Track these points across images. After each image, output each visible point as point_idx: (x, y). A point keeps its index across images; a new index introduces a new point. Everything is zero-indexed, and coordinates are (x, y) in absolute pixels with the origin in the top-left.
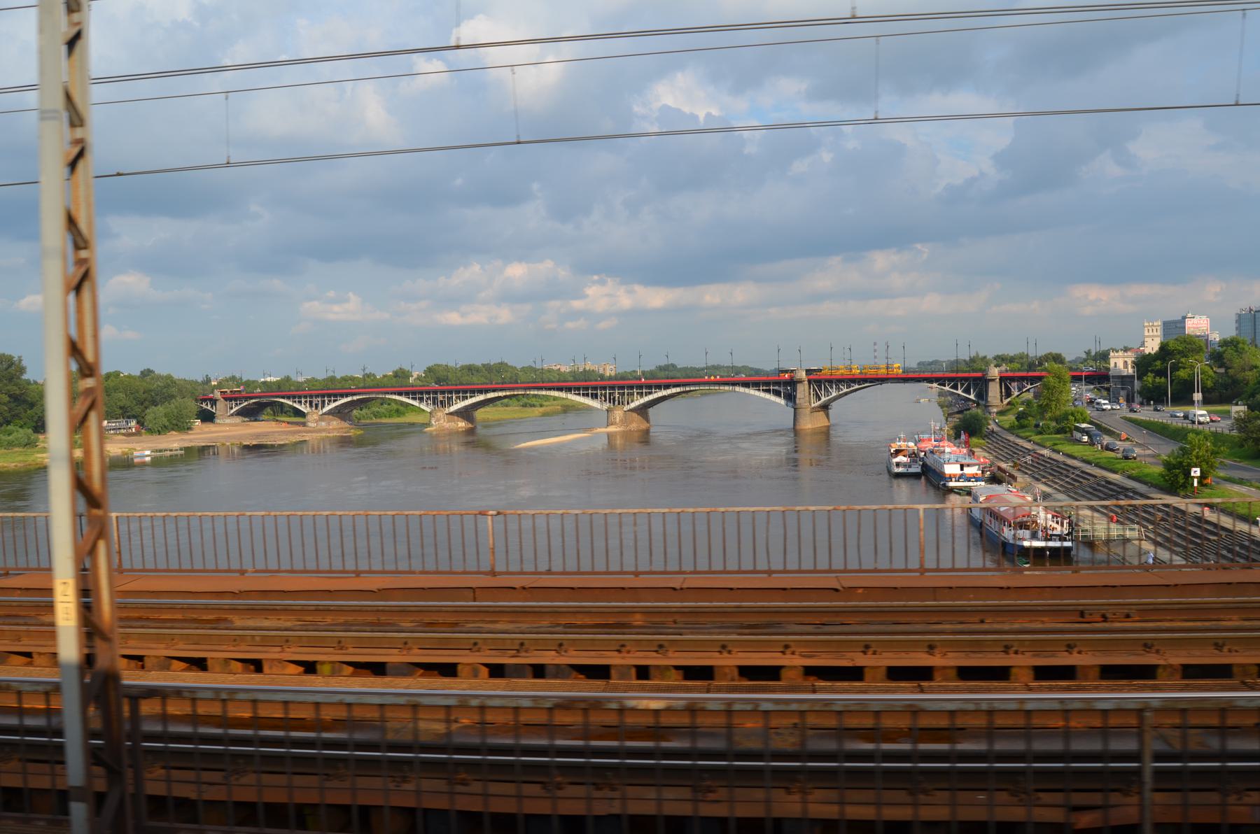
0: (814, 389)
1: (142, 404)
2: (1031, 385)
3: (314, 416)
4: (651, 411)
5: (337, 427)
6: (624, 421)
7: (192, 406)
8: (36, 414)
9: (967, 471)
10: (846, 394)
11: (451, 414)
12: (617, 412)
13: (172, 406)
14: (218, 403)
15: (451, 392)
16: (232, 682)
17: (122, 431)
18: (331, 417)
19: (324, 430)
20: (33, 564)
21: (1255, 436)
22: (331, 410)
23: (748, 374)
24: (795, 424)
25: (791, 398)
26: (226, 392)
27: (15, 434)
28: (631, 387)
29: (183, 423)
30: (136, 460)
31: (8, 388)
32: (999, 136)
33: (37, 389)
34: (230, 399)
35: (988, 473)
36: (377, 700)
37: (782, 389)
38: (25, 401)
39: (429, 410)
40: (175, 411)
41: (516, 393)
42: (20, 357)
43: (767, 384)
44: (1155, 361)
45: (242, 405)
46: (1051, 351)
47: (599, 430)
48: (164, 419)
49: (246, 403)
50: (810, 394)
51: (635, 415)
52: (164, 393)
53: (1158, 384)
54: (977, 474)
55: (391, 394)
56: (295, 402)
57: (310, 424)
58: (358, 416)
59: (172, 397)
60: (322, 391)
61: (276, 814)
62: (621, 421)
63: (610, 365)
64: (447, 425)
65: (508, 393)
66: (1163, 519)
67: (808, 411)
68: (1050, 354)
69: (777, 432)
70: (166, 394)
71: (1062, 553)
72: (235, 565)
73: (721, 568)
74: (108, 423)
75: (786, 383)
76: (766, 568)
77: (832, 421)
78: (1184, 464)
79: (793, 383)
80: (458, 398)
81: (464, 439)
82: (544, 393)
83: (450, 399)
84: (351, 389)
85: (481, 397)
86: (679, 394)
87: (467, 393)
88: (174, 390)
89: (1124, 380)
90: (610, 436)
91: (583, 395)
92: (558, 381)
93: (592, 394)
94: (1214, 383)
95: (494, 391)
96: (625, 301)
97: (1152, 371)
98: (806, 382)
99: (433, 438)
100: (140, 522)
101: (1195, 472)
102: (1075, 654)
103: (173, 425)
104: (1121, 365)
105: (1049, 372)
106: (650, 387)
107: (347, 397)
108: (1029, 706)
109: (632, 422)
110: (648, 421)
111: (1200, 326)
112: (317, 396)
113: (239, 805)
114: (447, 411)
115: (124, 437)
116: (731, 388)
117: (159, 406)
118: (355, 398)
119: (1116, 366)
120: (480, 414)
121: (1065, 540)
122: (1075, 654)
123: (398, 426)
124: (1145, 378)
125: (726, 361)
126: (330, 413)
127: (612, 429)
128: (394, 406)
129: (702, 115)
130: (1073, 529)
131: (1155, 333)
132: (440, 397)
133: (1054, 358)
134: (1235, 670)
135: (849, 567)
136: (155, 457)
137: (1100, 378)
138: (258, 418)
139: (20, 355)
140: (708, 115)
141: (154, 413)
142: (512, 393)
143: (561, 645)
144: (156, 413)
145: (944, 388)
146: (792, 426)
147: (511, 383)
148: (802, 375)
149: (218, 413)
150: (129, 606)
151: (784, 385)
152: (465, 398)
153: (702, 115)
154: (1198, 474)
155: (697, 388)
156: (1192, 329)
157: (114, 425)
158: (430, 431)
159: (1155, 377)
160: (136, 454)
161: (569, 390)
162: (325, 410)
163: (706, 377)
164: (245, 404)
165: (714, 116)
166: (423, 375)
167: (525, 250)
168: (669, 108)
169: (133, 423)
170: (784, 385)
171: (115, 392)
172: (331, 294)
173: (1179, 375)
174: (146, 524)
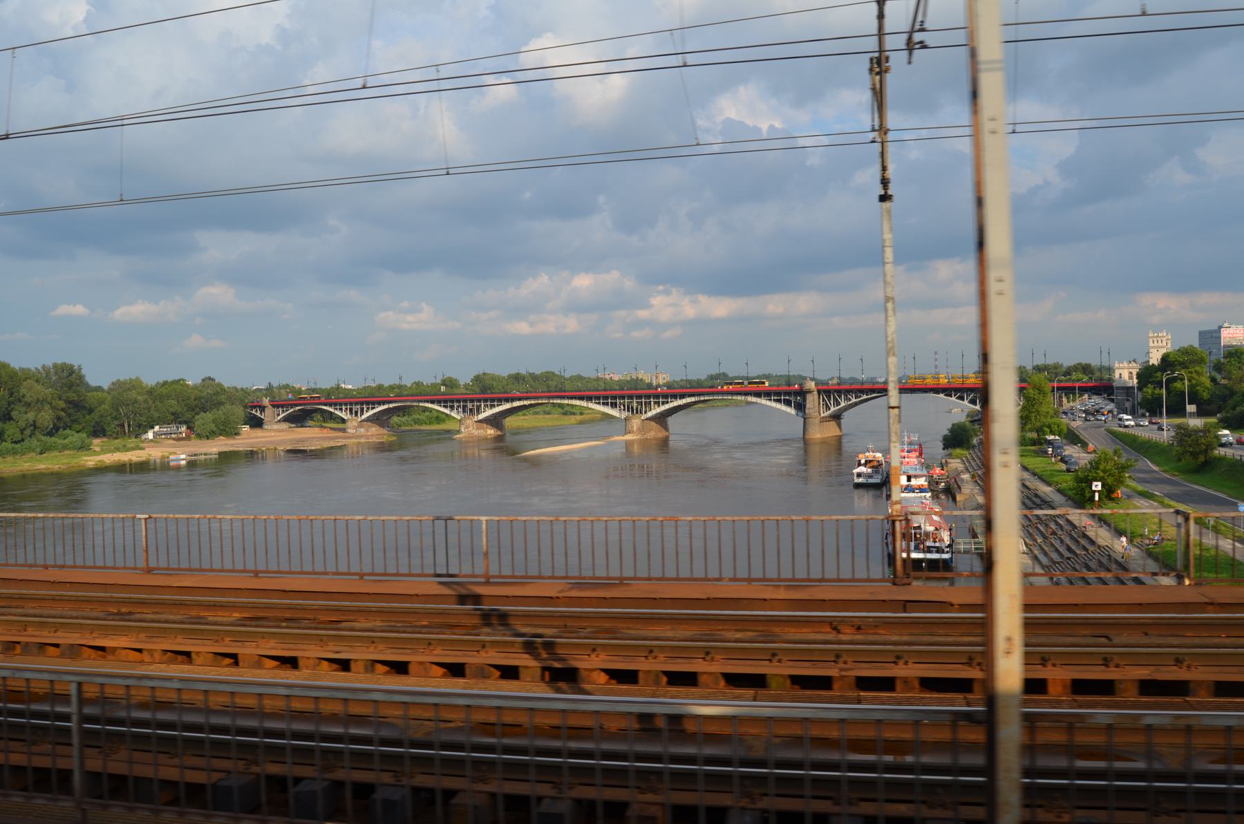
0: (824, 400)
1: (193, 410)
2: (867, 395)
3: (353, 422)
4: (670, 420)
5: (375, 434)
6: (642, 430)
8: (94, 419)
9: (914, 482)
10: (856, 404)
11: (480, 421)
13: (220, 413)
14: (266, 410)
15: (479, 401)
16: (188, 672)
17: (173, 436)
18: (369, 423)
19: (361, 436)
20: (79, 562)
21: (1191, 450)
22: (369, 417)
23: (521, 391)
24: (804, 434)
25: (800, 407)
27: (70, 437)
28: (648, 397)
29: (230, 428)
30: (172, 464)
31: (68, 394)
32: (1065, 146)
33: (97, 395)
34: (278, 407)
35: (943, 484)
36: (229, 688)
37: (792, 399)
38: (84, 408)
39: (459, 418)
40: (223, 417)
41: (540, 402)
42: (79, 366)
43: (778, 394)
44: (1156, 372)
45: (288, 412)
46: (1081, 361)
47: (616, 438)
48: (211, 424)
49: (292, 410)
50: (819, 404)
51: (653, 423)
52: (213, 400)
53: (1157, 396)
54: (922, 485)
55: (425, 402)
56: (337, 409)
57: (349, 430)
58: (399, 423)
59: (222, 404)
62: (639, 429)
63: (663, 374)
64: (476, 432)
65: (533, 402)
66: (1054, 533)
67: (817, 421)
68: (1079, 364)
69: (785, 441)
70: (216, 401)
72: (250, 566)
73: (849, 576)
74: (160, 428)
75: (797, 393)
76: (746, 576)
77: (844, 431)
78: (1090, 478)
79: (803, 393)
80: (486, 406)
81: (491, 445)
82: (566, 402)
83: (479, 408)
85: (507, 406)
86: (695, 403)
87: (494, 401)
88: (223, 398)
89: (1128, 390)
90: (628, 444)
91: (604, 404)
92: (605, 390)
93: (645, 402)
94: (1211, 396)
95: (520, 399)
96: (689, 310)
97: (1151, 383)
98: (816, 393)
99: (465, 443)
100: (123, 522)
101: (1096, 486)
102: (1050, 667)
103: (221, 430)
104: (1126, 376)
105: (1029, 384)
106: (666, 396)
107: (384, 404)
109: (650, 430)
111: (1237, 335)
112: (356, 404)
114: (476, 418)
115: (174, 442)
116: (743, 397)
117: (208, 413)
118: (391, 406)
119: (1121, 377)
120: (510, 422)
121: (943, 552)
122: (1050, 667)
123: (438, 433)
124: (1145, 390)
125: (589, 373)
126: (368, 419)
127: (629, 437)
128: (435, 414)
129: (764, 127)
130: (953, 541)
131: (1160, 344)
132: (469, 405)
133: (1083, 368)
135: (827, 576)
136: (190, 461)
137: (1105, 388)
138: (304, 424)
139: (79, 364)
140: (771, 127)
141: (203, 419)
142: (536, 402)
143: (838, 656)
144: (204, 420)
145: (950, 398)
146: (802, 436)
147: (556, 391)
148: (811, 385)
149: (266, 419)
150: (217, 604)
151: (794, 395)
152: (492, 406)
153: (764, 127)
154: (1099, 488)
155: (711, 398)
156: (1228, 339)
157: (165, 430)
158: (459, 437)
159: (1154, 388)
160: (172, 457)
161: (589, 399)
162: (363, 417)
163: (719, 387)
164: (290, 411)
165: (777, 128)
166: (471, 383)
167: (593, 261)
168: (733, 120)
169: (184, 428)
170: (794, 395)
171: (168, 399)
172: (406, 304)
173: (1176, 387)
174: (108, 525)
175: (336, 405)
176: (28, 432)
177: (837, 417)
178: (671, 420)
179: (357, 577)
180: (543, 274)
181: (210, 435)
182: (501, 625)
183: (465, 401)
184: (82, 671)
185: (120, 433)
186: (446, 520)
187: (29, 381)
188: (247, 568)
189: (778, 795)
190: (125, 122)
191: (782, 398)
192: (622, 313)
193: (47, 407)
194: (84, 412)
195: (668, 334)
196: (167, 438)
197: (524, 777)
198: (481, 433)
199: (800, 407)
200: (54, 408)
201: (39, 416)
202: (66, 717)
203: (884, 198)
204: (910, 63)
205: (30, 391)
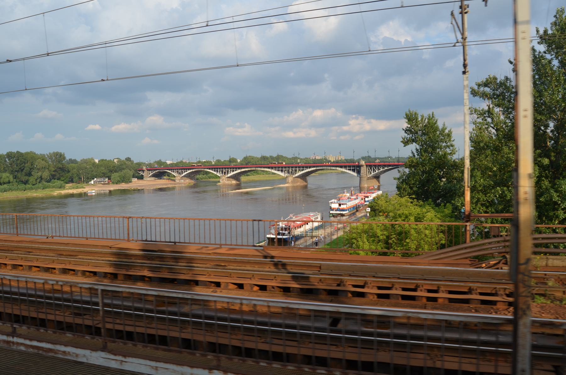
0: (369, 170)
5: (188, 181)
7: (131, 173)
11: (229, 177)
12: (289, 178)
14: (145, 172)
15: (228, 168)
17: (102, 183)
18: (186, 178)
24: (360, 185)
25: (359, 172)
26: (275, 163)
28: (296, 167)
42: (64, 153)
43: (350, 167)
51: (299, 179)
57: (176, 181)
60: (180, 167)
61: (368, 366)
62: (292, 182)
64: (227, 182)
65: (249, 169)
67: (365, 179)
71: (283, 241)
72: (85, 236)
79: (359, 166)
80: (299, 170)
84: (293, 164)
88: (124, 167)
90: (287, 188)
98: (365, 166)
108: (410, 315)
109: (298, 182)
110: (306, 182)
112: (180, 169)
113: (348, 361)
118: (193, 170)
126: (185, 176)
129: (402, 40)
132: (224, 170)
134: (291, 289)
140: (406, 40)
141: (115, 175)
142: (251, 169)
144: (115, 176)
150: (103, 252)
162: (183, 175)
165: (409, 41)
167: (322, 104)
169: (107, 179)
170: (357, 168)
172: (238, 124)
175: (172, 170)
176: (38, 181)
177: (377, 177)
178: (309, 178)
179: (173, 244)
180: (300, 110)
181: (117, 183)
182: (283, 269)
183: (222, 168)
184: (286, 299)
185: (80, 181)
186: (128, 218)
187: (39, 159)
188: (217, 243)
189: (362, 348)
190: (107, 45)
191: (280, 169)
192: (336, 128)
193: (47, 170)
194: (66, 172)
195: (357, 138)
196: (99, 184)
197: (325, 342)
198: (229, 182)
199: (359, 172)
200: (50, 171)
201: (43, 174)
202: (97, 304)
203: (464, 73)
204: (486, 6)
205: (39, 164)
